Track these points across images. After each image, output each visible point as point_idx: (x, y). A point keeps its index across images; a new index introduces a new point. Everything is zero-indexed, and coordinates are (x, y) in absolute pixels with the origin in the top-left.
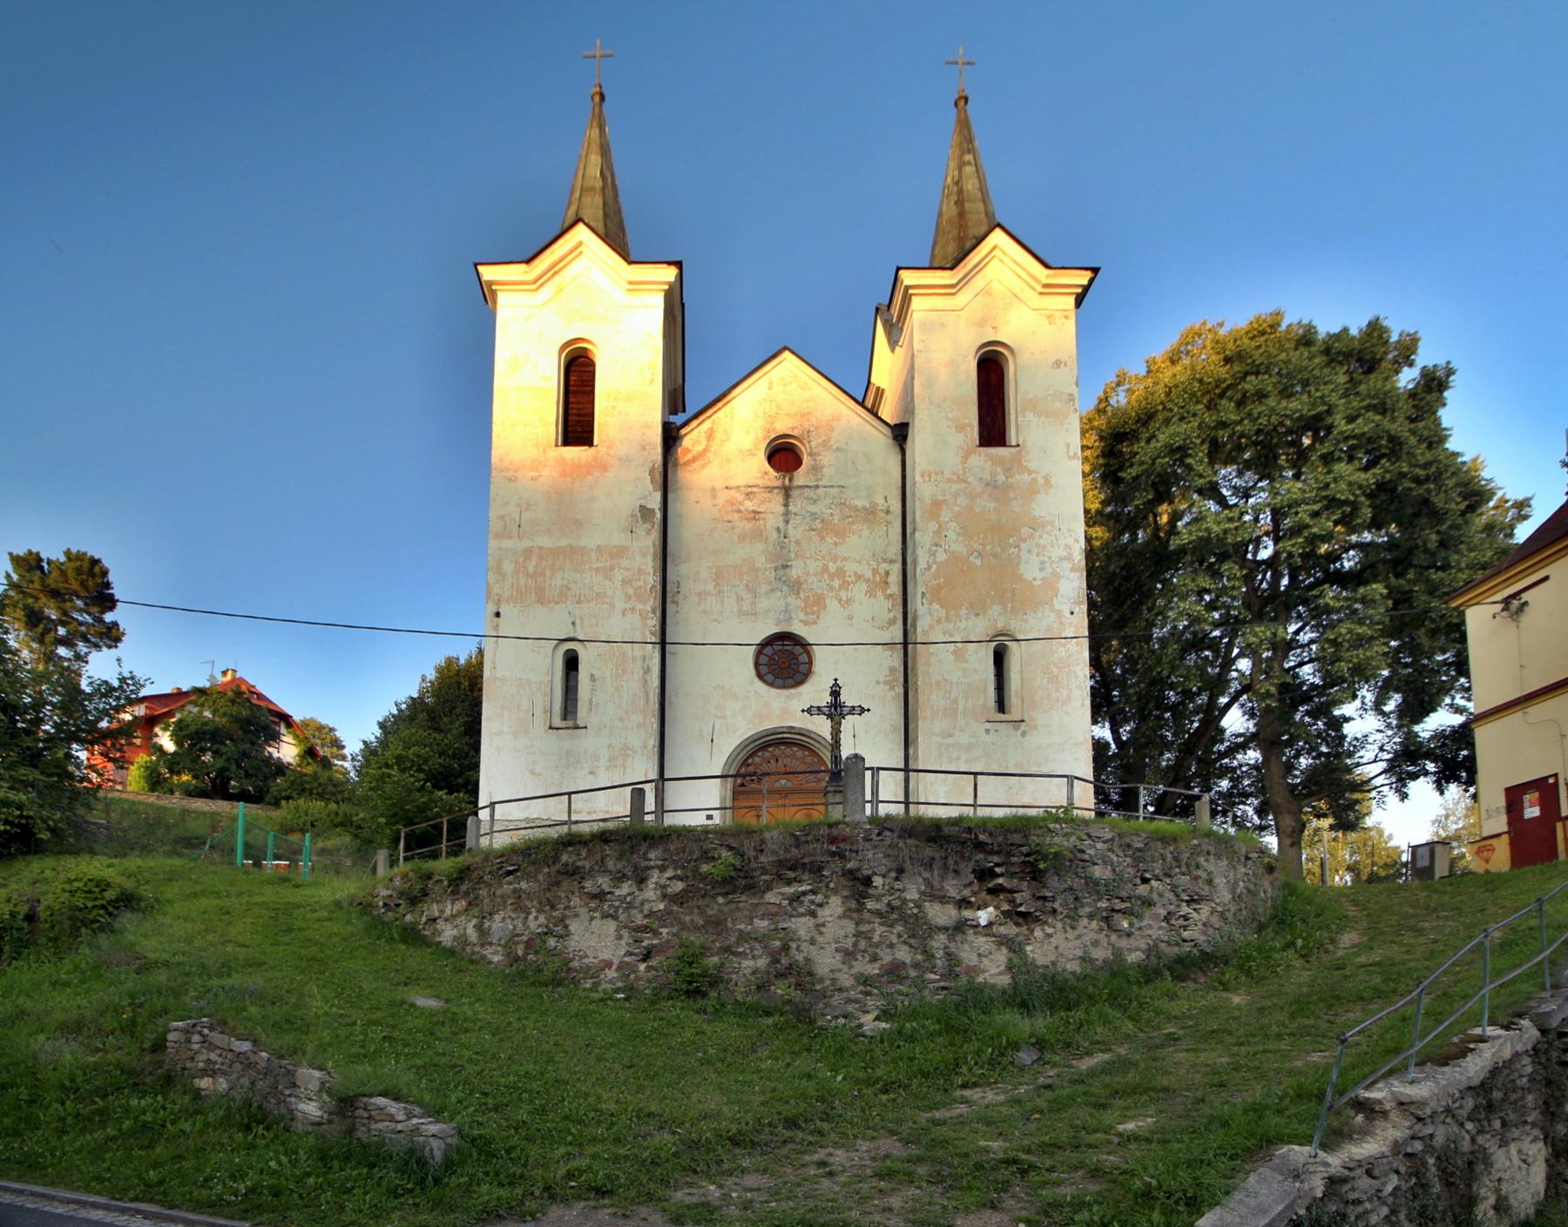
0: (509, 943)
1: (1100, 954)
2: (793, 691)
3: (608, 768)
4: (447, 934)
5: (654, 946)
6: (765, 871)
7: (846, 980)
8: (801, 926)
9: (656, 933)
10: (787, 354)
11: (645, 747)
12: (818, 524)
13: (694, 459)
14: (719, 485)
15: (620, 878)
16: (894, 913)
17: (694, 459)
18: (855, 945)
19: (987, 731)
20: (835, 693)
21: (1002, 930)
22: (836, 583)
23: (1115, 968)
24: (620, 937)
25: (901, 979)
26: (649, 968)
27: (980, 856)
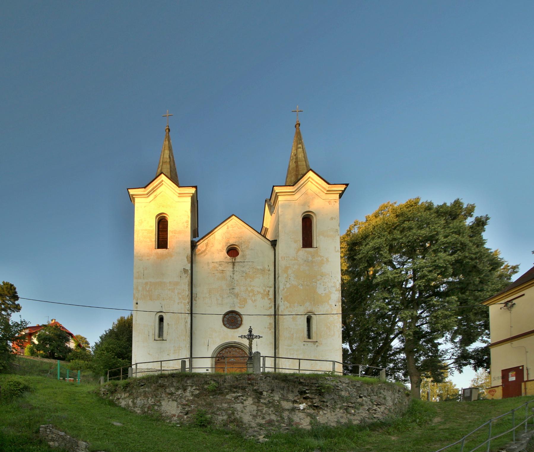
0: (143, 407)
1: (343, 421)
4: (123, 403)
6: (226, 388)
7: (253, 424)
8: (239, 406)
9: (190, 406)
11: (186, 347)
12: (244, 275)
13: (202, 253)
14: (210, 261)
15: (178, 389)
16: (270, 404)
17: (202, 253)
18: (257, 413)
19: (304, 345)
20: (250, 331)
21: (308, 411)
22: (251, 294)
23: (349, 426)
24: (178, 407)
25: (273, 425)
26: (187, 417)
27: (301, 387)
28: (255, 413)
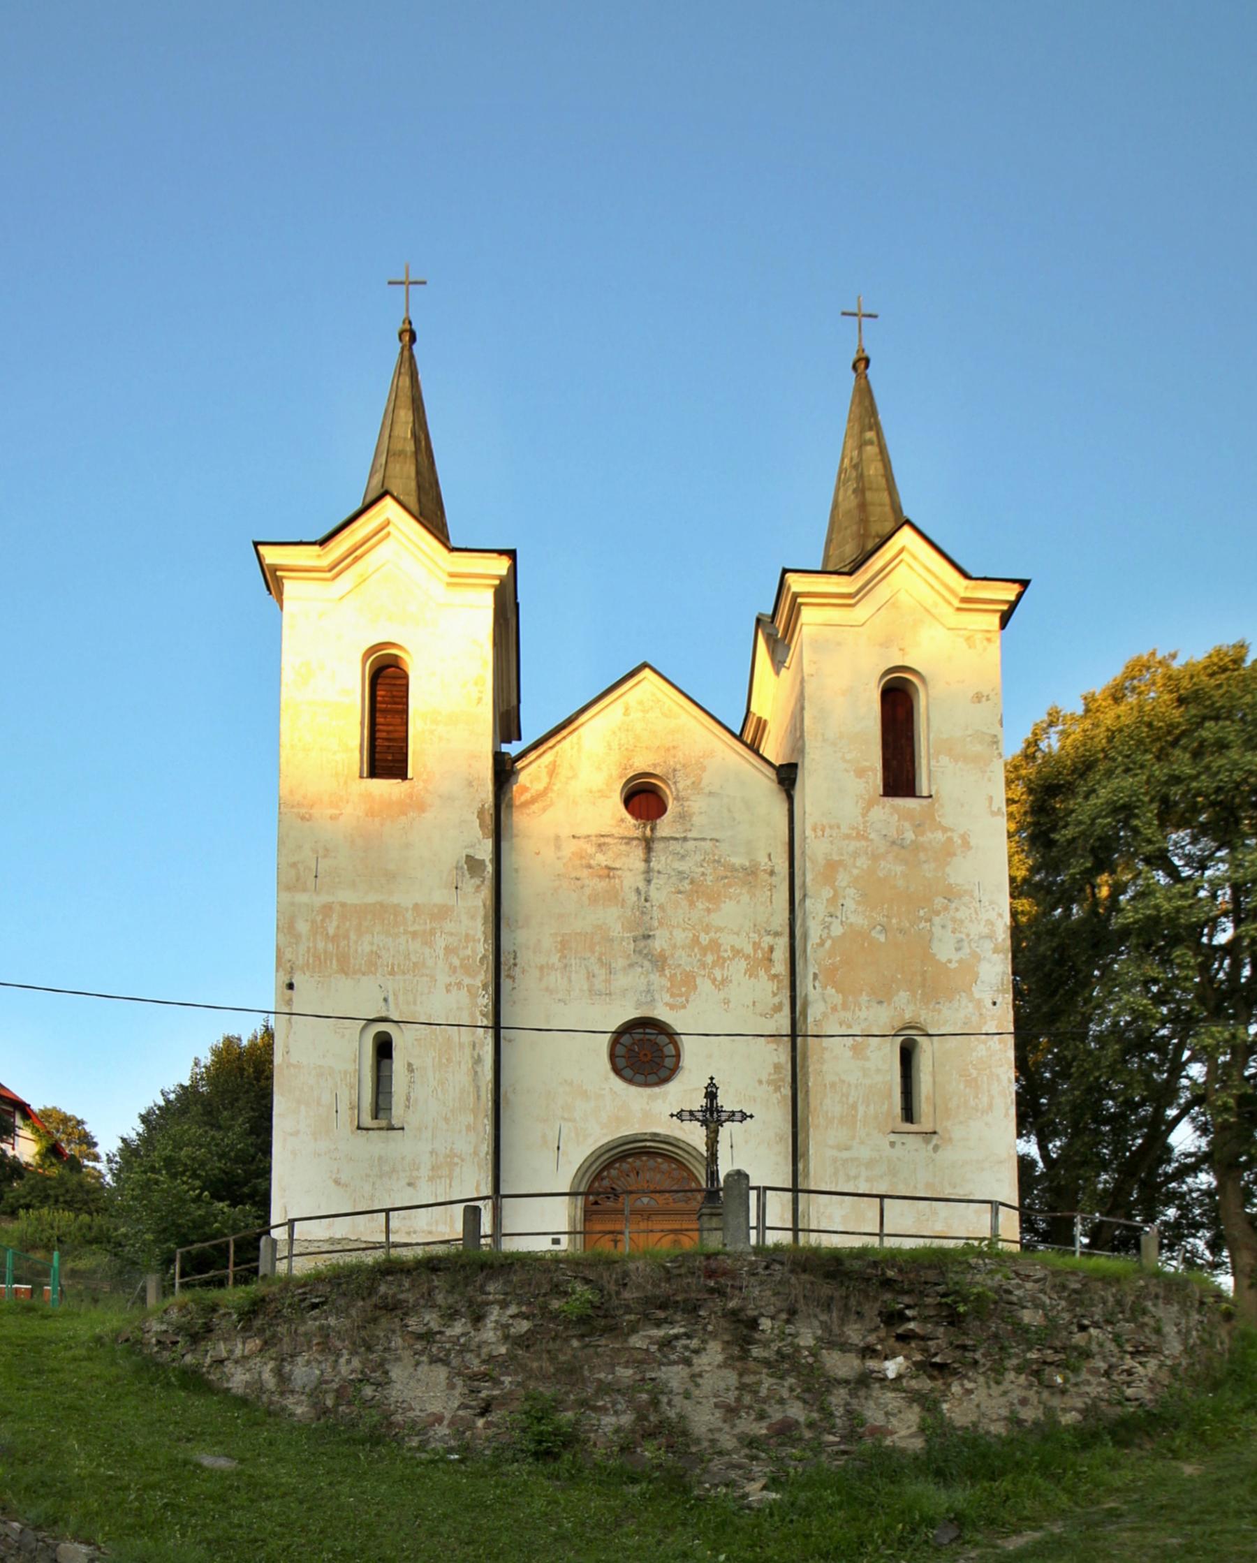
0: (314, 1394)
2: (656, 1090)
3: (431, 1179)
4: (238, 1379)
5: (494, 1398)
6: (628, 1310)
7: (728, 1442)
8: (674, 1376)
9: (497, 1382)
10: (647, 672)
11: (476, 1153)
12: (686, 886)
13: (533, 800)
14: (565, 832)
15: (451, 1315)
17: (533, 800)
18: (738, 1399)
19: (892, 1144)
20: (711, 1095)
22: (709, 959)
23: (1047, 1430)
24: (451, 1386)
25: (795, 1442)
26: (488, 1425)
27: (888, 1296)
28: (731, 1398)
